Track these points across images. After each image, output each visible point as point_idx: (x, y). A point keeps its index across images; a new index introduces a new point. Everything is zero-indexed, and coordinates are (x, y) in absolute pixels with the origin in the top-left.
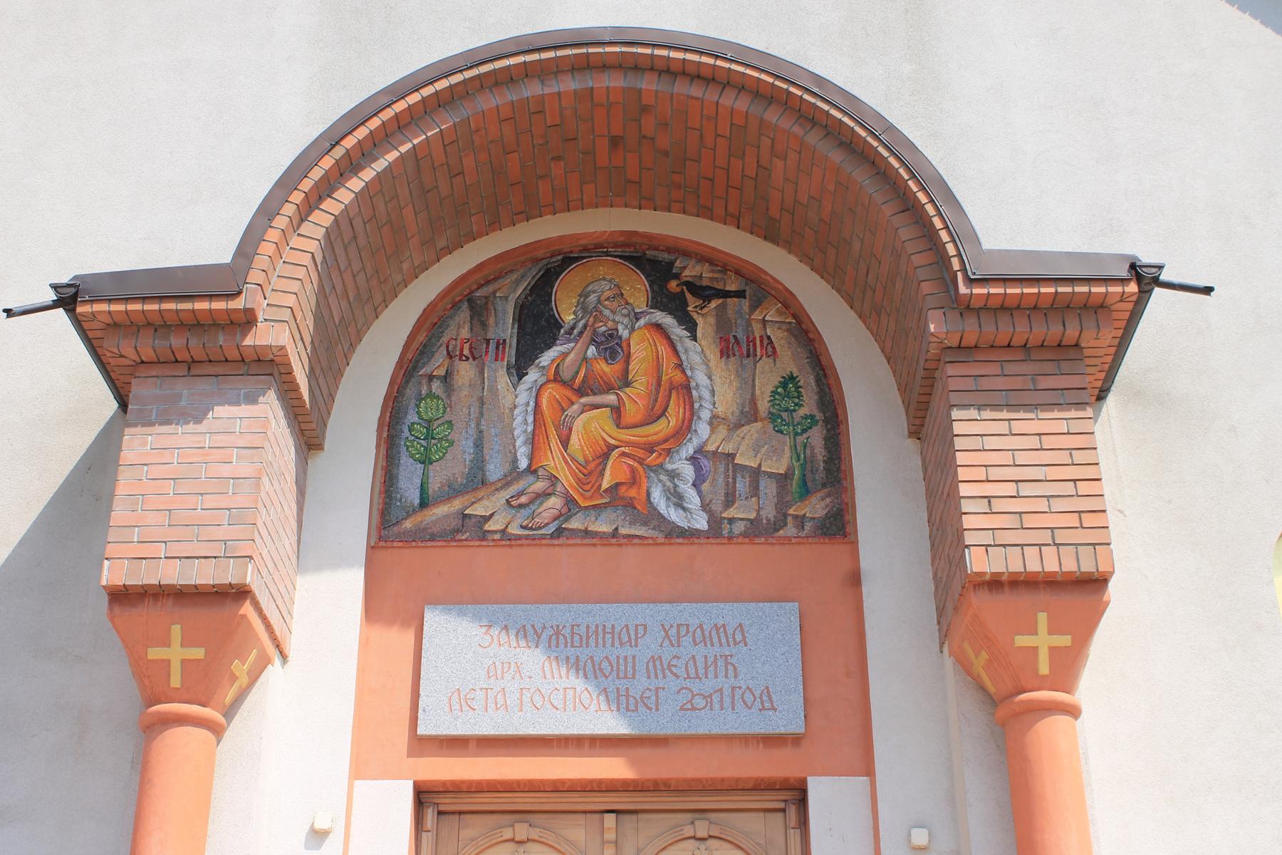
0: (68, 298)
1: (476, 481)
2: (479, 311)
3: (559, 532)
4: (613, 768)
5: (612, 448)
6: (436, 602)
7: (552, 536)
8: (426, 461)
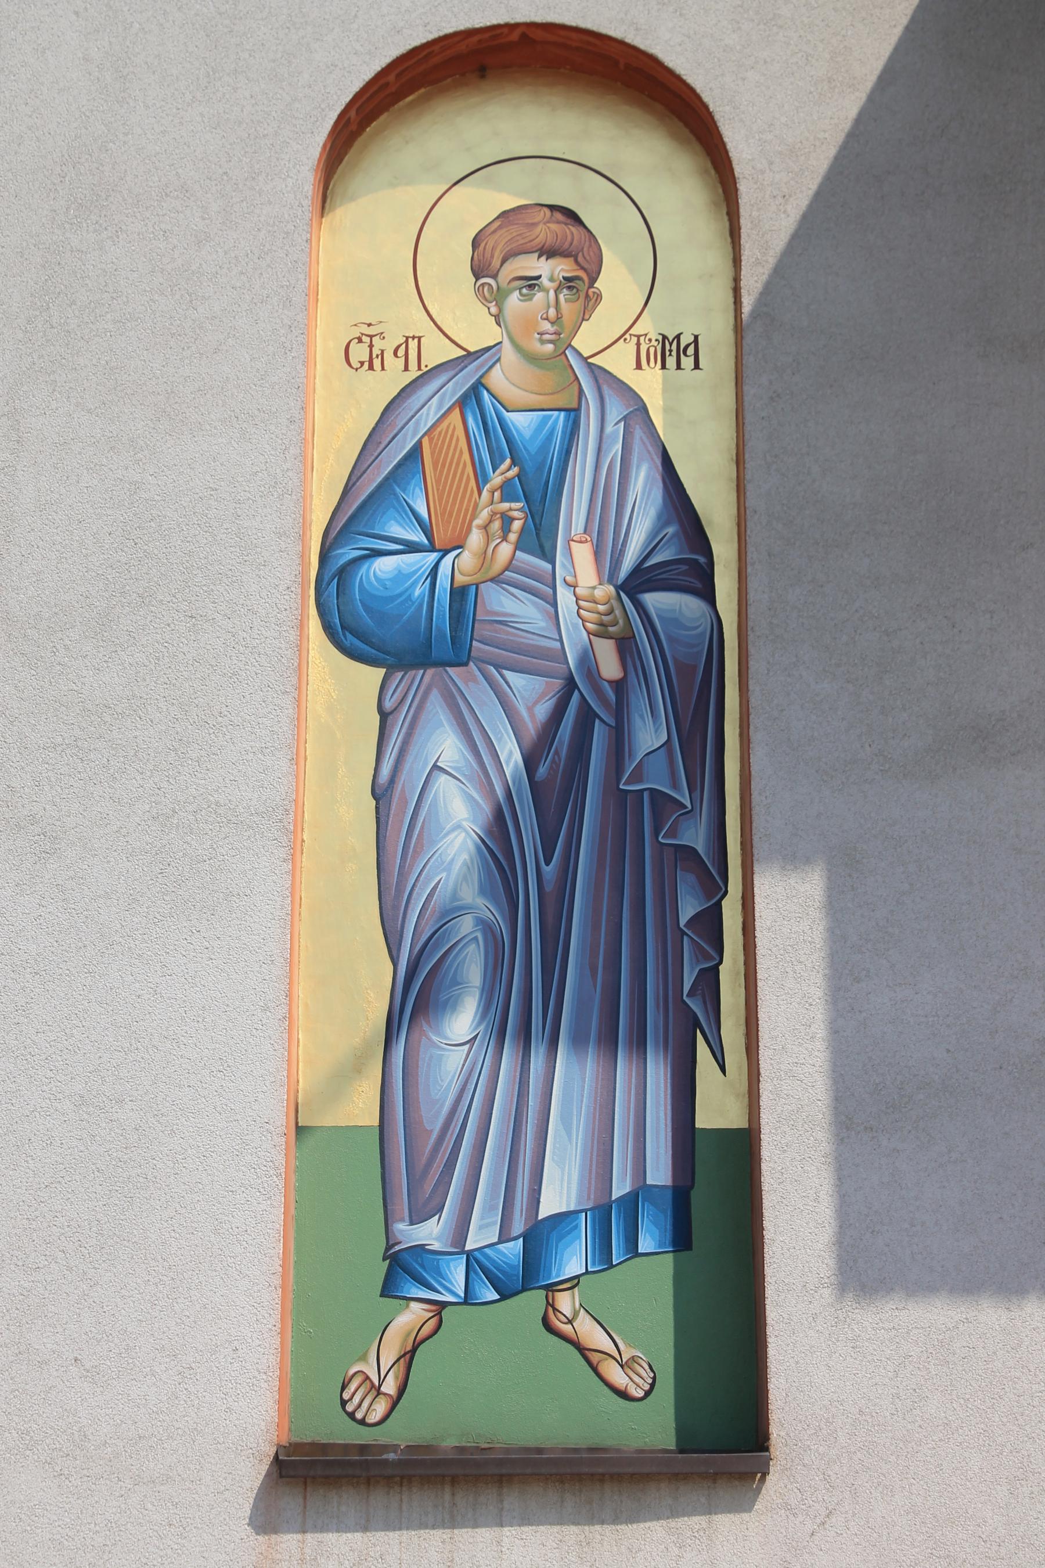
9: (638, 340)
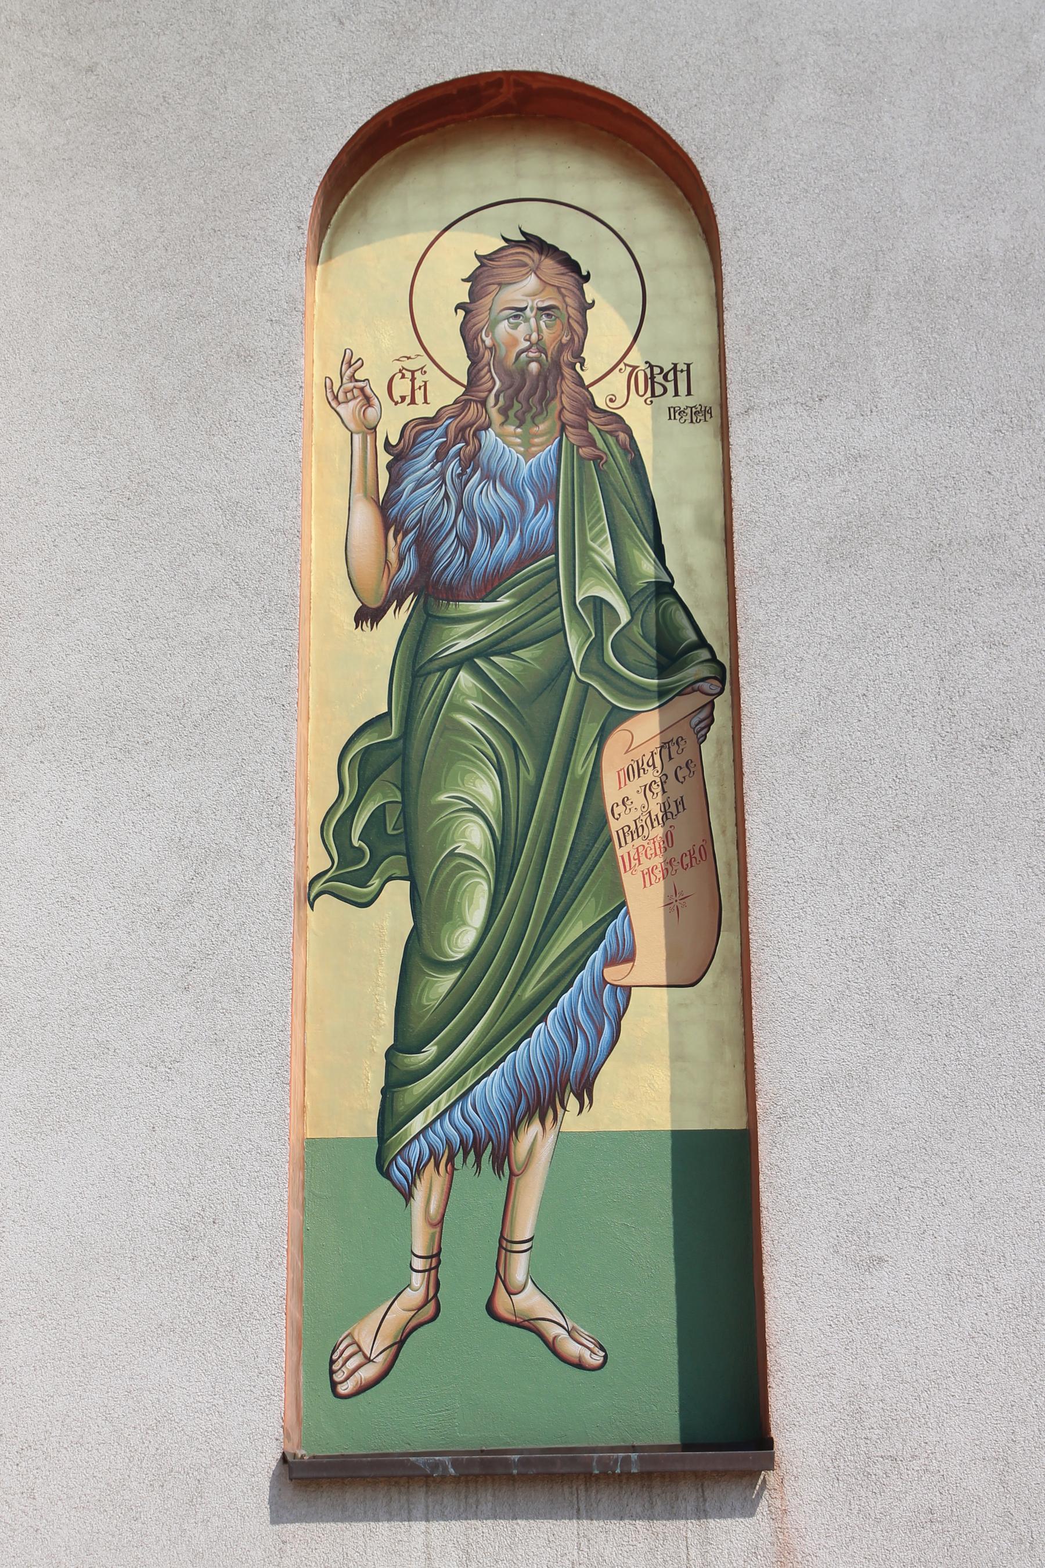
9: (413, 375)
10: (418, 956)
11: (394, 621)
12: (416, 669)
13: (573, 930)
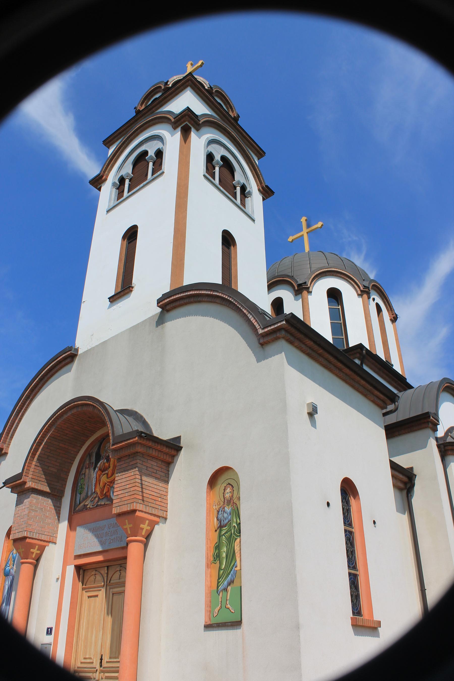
0: (5, 484)
1: (87, 497)
2: (90, 456)
3: (97, 506)
4: (100, 558)
5: (106, 483)
6: (79, 525)
7: (96, 507)
8: (80, 494)
10: (220, 569)
11: (218, 531)
12: (220, 536)
13: (232, 564)
